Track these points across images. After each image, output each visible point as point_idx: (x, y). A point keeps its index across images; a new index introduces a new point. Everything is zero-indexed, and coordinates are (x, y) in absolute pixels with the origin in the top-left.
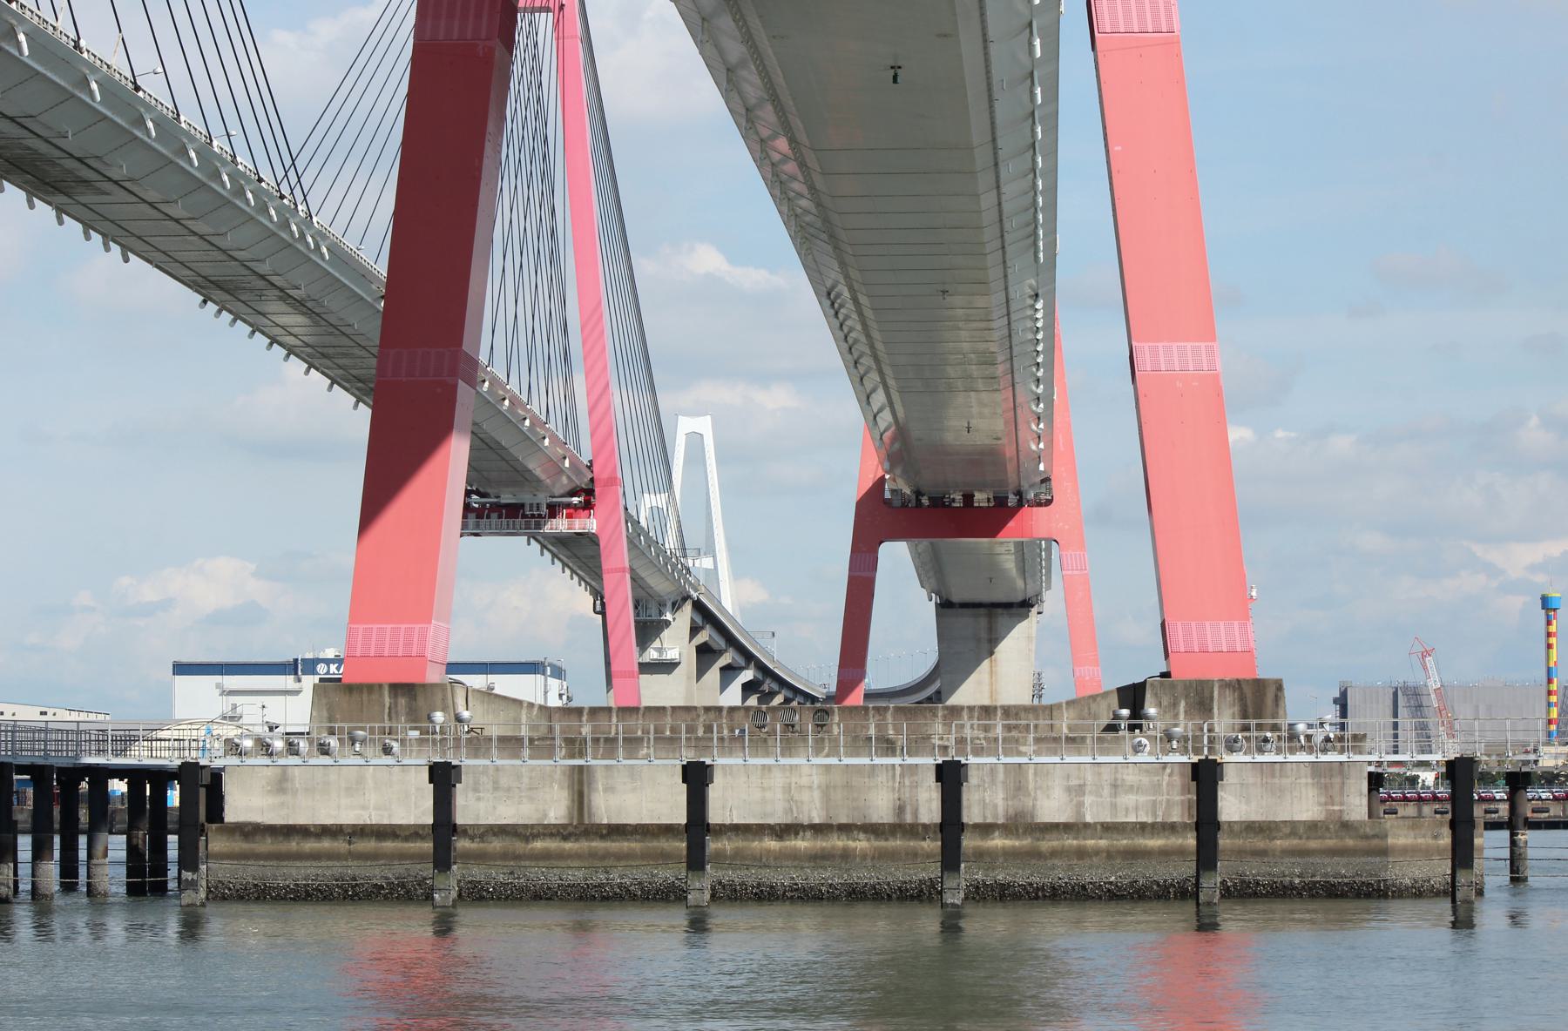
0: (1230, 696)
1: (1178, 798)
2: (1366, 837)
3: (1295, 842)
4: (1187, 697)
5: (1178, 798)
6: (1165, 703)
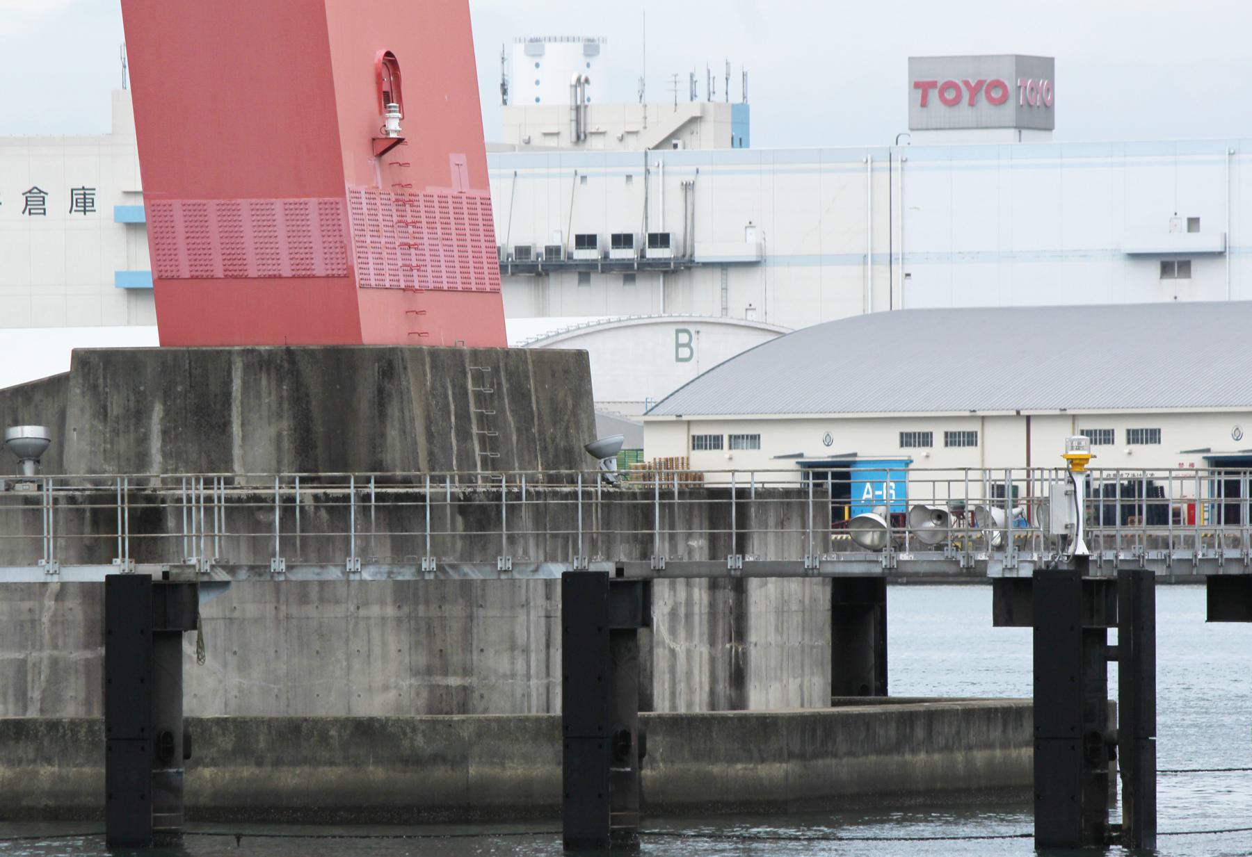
0: (269, 392)
1: (78, 655)
2: (415, 760)
3: (247, 771)
4: (167, 395)
5: (78, 655)
6: (115, 409)
